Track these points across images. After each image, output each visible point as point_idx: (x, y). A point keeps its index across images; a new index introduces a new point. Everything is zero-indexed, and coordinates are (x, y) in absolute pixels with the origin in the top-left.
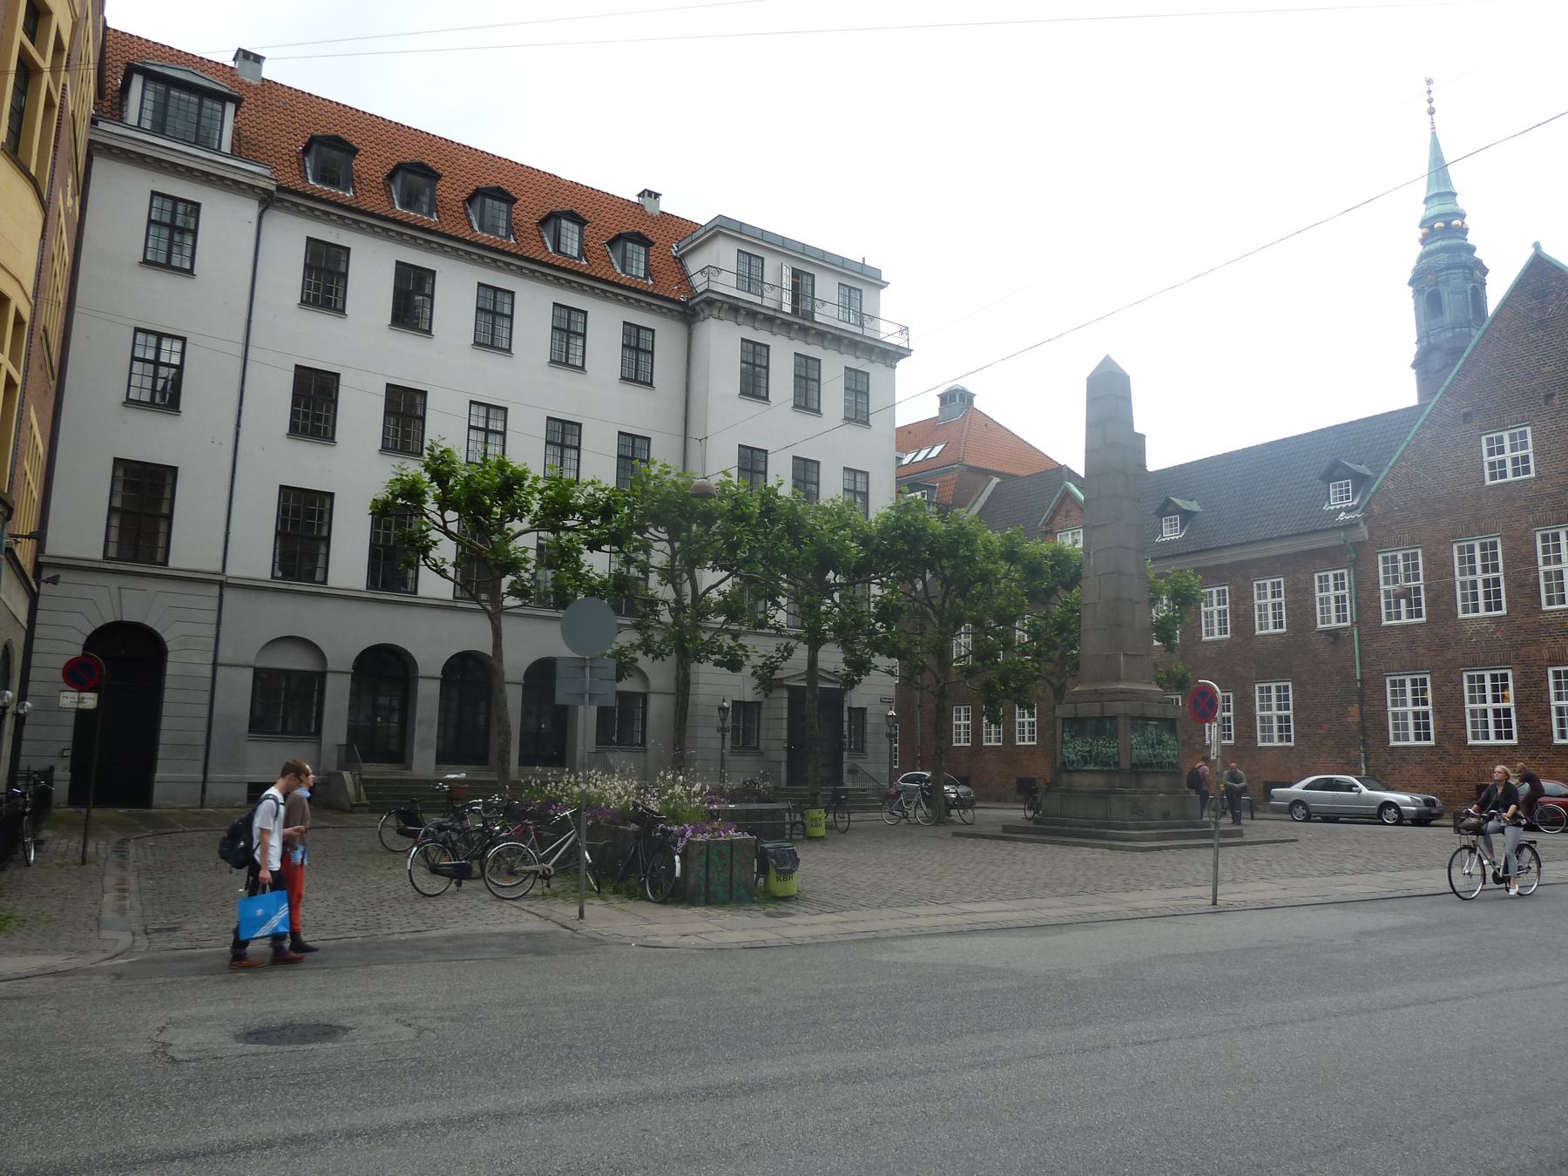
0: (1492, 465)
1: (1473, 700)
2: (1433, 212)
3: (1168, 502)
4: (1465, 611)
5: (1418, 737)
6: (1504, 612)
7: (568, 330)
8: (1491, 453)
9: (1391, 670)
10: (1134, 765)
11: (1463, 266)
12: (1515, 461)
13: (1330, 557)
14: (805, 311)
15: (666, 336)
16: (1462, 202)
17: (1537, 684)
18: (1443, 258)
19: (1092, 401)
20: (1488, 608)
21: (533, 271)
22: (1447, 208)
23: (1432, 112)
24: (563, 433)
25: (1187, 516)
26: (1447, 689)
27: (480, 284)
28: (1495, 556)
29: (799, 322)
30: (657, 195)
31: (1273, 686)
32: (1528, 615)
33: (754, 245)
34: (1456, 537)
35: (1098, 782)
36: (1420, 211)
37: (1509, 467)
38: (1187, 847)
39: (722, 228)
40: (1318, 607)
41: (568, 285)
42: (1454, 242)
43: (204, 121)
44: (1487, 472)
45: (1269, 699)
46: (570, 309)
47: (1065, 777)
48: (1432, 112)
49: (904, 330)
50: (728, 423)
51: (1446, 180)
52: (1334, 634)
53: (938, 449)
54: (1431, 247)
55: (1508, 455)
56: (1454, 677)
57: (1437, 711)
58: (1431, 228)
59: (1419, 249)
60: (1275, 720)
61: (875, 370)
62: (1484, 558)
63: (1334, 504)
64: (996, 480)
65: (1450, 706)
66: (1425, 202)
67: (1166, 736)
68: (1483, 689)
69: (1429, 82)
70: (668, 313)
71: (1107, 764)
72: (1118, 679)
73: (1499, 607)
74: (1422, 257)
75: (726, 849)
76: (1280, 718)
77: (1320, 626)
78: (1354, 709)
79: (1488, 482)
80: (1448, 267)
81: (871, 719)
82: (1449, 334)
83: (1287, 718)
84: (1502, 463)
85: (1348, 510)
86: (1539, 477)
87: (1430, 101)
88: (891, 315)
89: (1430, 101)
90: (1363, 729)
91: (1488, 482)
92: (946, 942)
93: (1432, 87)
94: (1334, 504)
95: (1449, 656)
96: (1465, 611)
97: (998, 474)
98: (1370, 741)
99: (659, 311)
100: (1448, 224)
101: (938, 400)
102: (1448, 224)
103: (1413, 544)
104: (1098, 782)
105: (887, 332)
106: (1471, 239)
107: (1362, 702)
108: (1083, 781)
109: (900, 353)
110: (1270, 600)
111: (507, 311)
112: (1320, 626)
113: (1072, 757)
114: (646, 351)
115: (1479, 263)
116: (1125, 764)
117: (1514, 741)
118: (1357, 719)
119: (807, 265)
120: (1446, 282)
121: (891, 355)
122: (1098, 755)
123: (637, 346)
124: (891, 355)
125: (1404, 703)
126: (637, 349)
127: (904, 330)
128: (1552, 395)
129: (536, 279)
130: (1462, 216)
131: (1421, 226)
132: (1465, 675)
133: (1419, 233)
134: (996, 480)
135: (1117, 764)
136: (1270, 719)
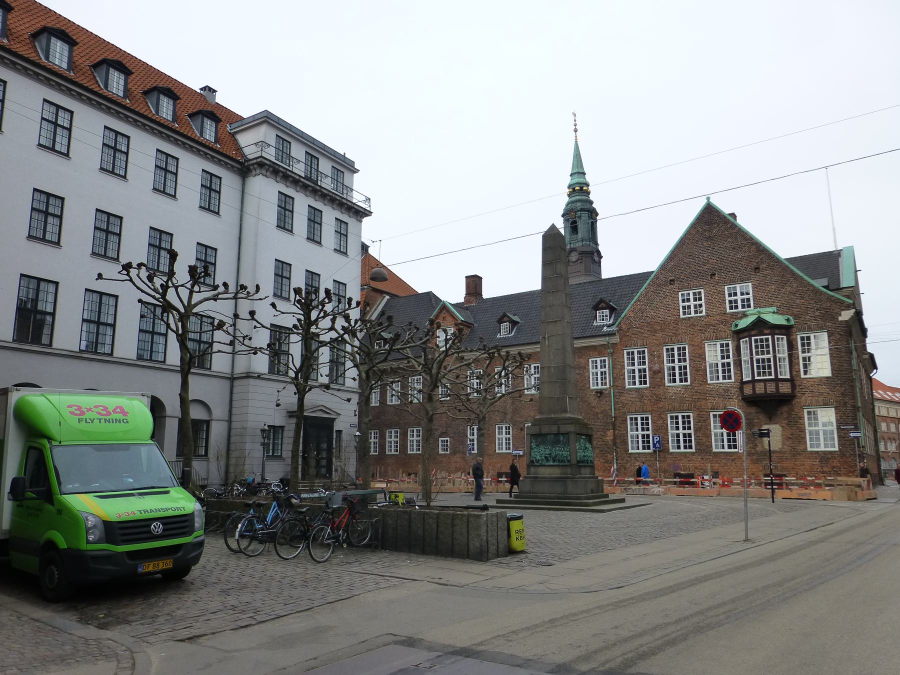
1: (632, 430)
3: (505, 315)
5: (644, 448)
6: (689, 383)
7: (166, 170)
8: (683, 301)
9: (630, 412)
10: (578, 462)
11: (588, 211)
12: (743, 301)
14: (317, 181)
15: (229, 181)
16: (588, 178)
17: (699, 421)
18: (579, 205)
19: (545, 249)
20: (641, 384)
21: (144, 125)
22: (582, 180)
23: (576, 131)
24: (160, 239)
25: (514, 323)
26: (660, 422)
28: (684, 354)
29: (309, 186)
30: (215, 91)
31: (680, 415)
32: (701, 385)
33: (287, 134)
34: (666, 344)
35: (556, 472)
36: (568, 180)
37: (740, 304)
39: (267, 119)
41: (168, 138)
42: (584, 198)
46: (168, 155)
47: (532, 469)
48: (576, 131)
50: (259, 241)
52: (600, 393)
54: (573, 199)
55: (692, 303)
56: (663, 416)
58: (574, 189)
59: (566, 199)
62: (679, 355)
63: (598, 322)
64: (387, 297)
65: (661, 430)
66: (571, 175)
67: (588, 445)
68: (637, 424)
69: (575, 115)
70: (231, 168)
72: (565, 411)
73: (686, 380)
75: (495, 519)
78: (610, 433)
79: (682, 316)
80: (581, 210)
81: (344, 437)
82: (580, 244)
84: (736, 301)
85: (609, 326)
86: (708, 315)
87: (575, 125)
88: (361, 189)
89: (575, 125)
90: (615, 444)
91: (682, 316)
94: (598, 322)
95: (661, 405)
97: (388, 294)
98: (618, 450)
99: (225, 166)
100: (581, 188)
102: (581, 188)
103: (643, 346)
104: (556, 472)
105: (357, 198)
106: (591, 197)
107: (614, 429)
109: (366, 213)
111: (124, 149)
113: (538, 458)
114: (215, 191)
115: (594, 210)
116: (574, 462)
117: (693, 450)
118: (612, 438)
119: (316, 150)
120: (580, 217)
121: (360, 213)
122: (556, 456)
123: (210, 189)
124: (360, 213)
126: (210, 189)
128: (714, 275)
129: (146, 130)
130: (588, 185)
131: (569, 188)
132: (669, 415)
134: (387, 297)
135: (569, 461)
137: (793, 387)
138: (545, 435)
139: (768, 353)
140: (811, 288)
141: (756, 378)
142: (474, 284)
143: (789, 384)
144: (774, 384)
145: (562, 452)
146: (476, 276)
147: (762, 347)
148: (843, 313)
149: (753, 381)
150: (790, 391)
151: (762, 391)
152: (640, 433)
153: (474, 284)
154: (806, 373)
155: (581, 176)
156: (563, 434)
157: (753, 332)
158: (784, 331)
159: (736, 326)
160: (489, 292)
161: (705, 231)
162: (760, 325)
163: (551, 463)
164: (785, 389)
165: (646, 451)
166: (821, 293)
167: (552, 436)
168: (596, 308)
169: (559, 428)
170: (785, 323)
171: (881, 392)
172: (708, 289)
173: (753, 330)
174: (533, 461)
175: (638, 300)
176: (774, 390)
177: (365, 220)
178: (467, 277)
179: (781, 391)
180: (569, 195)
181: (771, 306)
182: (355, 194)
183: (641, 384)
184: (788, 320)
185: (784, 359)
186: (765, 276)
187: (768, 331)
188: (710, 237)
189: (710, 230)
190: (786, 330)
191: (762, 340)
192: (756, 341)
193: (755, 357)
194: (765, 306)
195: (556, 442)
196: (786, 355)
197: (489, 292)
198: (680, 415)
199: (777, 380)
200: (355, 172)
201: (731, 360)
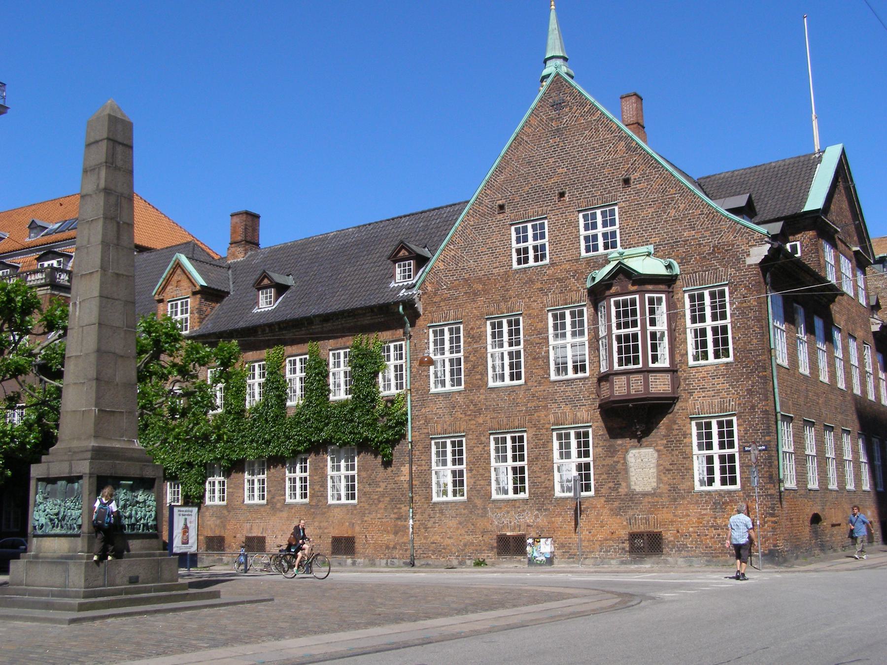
57: (470, 470)
113: (43, 520)
118: (407, 478)
141: (616, 367)
142: (248, 226)
143: (668, 377)
144: (640, 377)
151: (624, 391)
158: (662, 287)
159: (594, 279)
163: (57, 531)
164: (660, 386)
167: (64, 482)
170: (663, 271)
175: (451, 242)
176: (641, 388)
181: (647, 243)
183: (512, 379)
184: (669, 267)
188: (558, 130)
191: (625, 303)
193: (615, 332)
194: (638, 245)
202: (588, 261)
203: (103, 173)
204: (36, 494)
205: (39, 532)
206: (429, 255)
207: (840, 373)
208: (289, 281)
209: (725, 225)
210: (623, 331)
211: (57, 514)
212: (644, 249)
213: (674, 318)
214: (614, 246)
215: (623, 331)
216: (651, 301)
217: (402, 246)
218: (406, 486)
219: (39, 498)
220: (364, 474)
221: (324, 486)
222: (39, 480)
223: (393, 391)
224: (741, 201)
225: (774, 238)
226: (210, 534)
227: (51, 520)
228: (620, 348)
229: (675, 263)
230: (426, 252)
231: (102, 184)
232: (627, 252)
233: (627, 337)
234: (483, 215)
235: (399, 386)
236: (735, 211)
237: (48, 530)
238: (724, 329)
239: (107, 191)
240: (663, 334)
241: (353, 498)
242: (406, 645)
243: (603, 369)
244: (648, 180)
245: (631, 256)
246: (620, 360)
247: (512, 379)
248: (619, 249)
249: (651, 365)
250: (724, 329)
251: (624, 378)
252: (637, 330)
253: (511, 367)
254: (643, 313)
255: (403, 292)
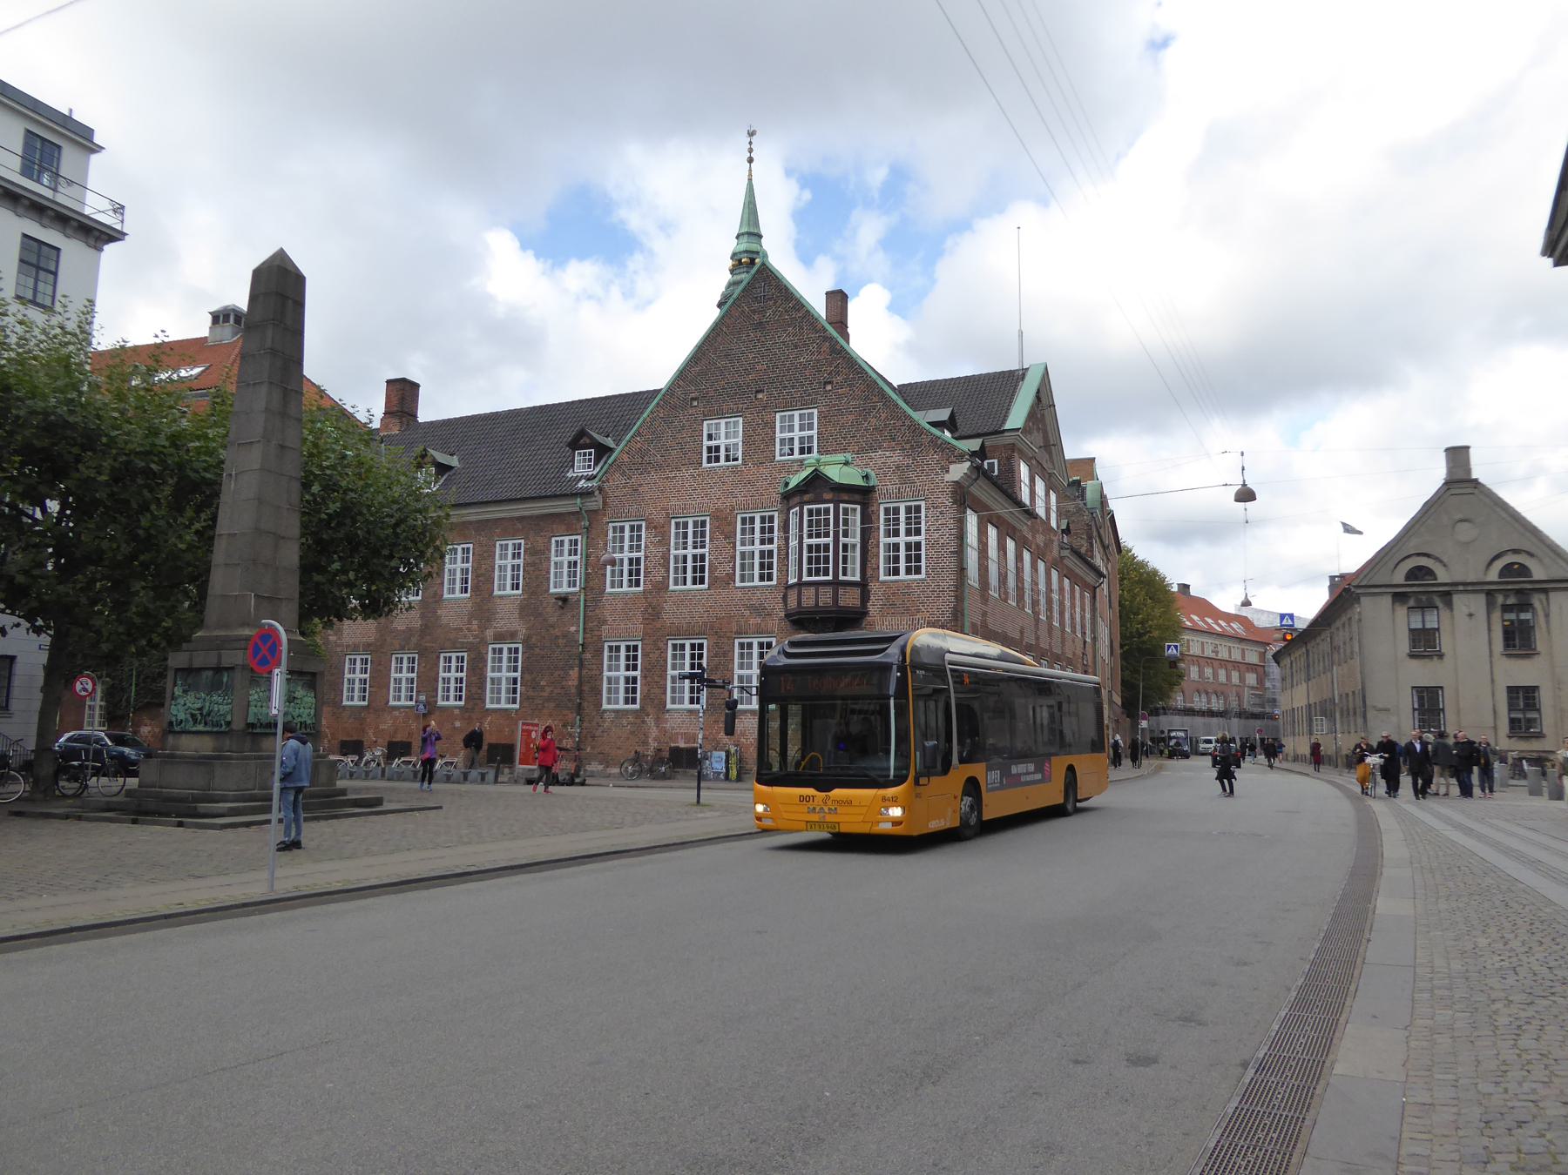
0: (710, 449)
2: (743, 247)
4: (676, 583)
5: (627, 702)
13: (565, 522)
22: (754, 247)
23: (750, 160)
27: (25, 236)
31: (688, 644)
35: (205, 745)
36: (731, 245)
38: (248, 825)
40: (552, 570)
43: (1217, 705)
44: (705, 455)
45: (500, 660)
47: (171, 739)
48: (750, 160)
49: (119, 209)
51: (757, 224)
52: (564, 599)
53: (197, 370)
54: (738, 278)
57: (644, 677)
59: (727, 277)
60: (622, 681)
61: (72, 250)
71: (218, 725)
74: (731, 284)
76: (627, 680)
77: (552, 590)
78: (574, 673)
83: (635, 679)
87: (751, 151)
89: (751, 151)
90: (580, 693)
92: (86, 916)
93: (754, 139)
96: (676, 583)
98: (585, 704)
101: (210, 317)
104: (205, 745)
105: (95, 207)
107: (581, 666)
108: (190, 745)
110: (509, 562)
112: (552, 590)
113: (182, 716)
116: (238, 725)
118: (576, 683)
125: (618, 669)
127: (119, 209)
133: (730, 263)
135: (228, 723)
136: (617, 680)
137: (865, 597)
138: (200, 670)
139: (827, 535)
140: (908, 423)
141: (805, 578)
142: (403, 394)
143: (858, 591)
144: (829, 590)
145: (220, 705)
146: (404, 380)
147: (818, 521)
148: (952, 467)
149: (800, 584)
150: (858, 603)
151: (812, 603)
152: (623, 673)
153: (403, 394)
154: (845, 574)
155: (753, 239)
156: (227, 669)
157: (806, 497)
158: (857, 497)
159: (787, 484)
160: (429, 411)
161: (754, 312)
162: (816, 484)
163: (201, 728)
164: (850, 599)
165: (630, 706)
166: (922, 431)
167: (210, 673)
168: (575, 444)
169: (220, 657)
170: (861, 482)
171: (1195, 618)
172: (750, 417)
173: (806, 492)
174: (171, 723)
175: (638, 433)
176: (830, 601)
177: (110, 249)
178: (388, 382)
179: (841, 603)
180: (732, 272)
181: (845, 450)
182: (90, 198)
183: (694, 583)
184: (866, 477)
185: (854, 546)
186: (839, 397)
187: (827, 496)
188: (760, 323)
189: (762, 312)
190: (863, 495)
191: (818, 512)
192: (810, 512)
193: (806, 541)
194: (835, 452)
195: (215, 686)
196: (857, 540)
197: (429, 411)
198: (688, 644)
199: (836, 584)
200: (93, 151)
201: (774, 547)
202: (783, 464)
203: (269, 333)
204: (175, 685)
205: (177, 729)
206: (612, 445)
207: (1056, 615)
208: (454, 461)
209: (925, 440)
210: (814, 541)
211: (200, 709)
212: (840, 457)
213: (867, 534)
214: (810, 450)
215: (814, 541)
216: (846, 511)
217: (582, 433)
218: (573, 690)
219: (178, 691)
220: (527, 677)
221: (482, 686)
222: (177, 670)
223: (565, 589)
224: (943, 414)
225: (974, 454)
226: (493, 741)
227: (193, 715)
228: (810, 559)
229: (873, 474)
230: (610, 442)
231: (269, 343)
232: (825, 458)
233: (818, 546)
234: (674, 408)
235: (572, 584)
236: (934, 424)
237: (190, 727)
238: (918, 545)
239: (273, 352)
240: (854, 546)
241: (514, 702)
242: (683, 845)
243: (792, 581)
244: (850, 386)
245: (826, 464)
246: (810, 570)
247: (694, 583)
248: (815, 454)
249: (841, 578)
250: (918, 545)
251: (812, 589)
252: (830, 540)
253: (694, 571)
254: (836, 524)
255: (582, 484)
